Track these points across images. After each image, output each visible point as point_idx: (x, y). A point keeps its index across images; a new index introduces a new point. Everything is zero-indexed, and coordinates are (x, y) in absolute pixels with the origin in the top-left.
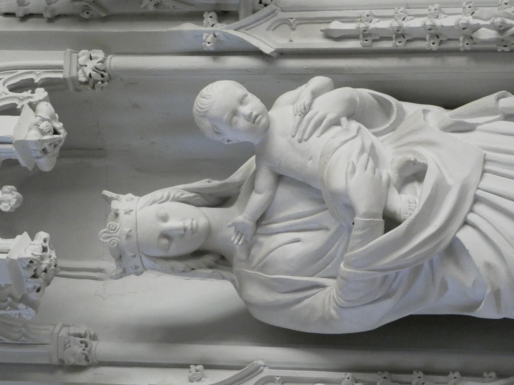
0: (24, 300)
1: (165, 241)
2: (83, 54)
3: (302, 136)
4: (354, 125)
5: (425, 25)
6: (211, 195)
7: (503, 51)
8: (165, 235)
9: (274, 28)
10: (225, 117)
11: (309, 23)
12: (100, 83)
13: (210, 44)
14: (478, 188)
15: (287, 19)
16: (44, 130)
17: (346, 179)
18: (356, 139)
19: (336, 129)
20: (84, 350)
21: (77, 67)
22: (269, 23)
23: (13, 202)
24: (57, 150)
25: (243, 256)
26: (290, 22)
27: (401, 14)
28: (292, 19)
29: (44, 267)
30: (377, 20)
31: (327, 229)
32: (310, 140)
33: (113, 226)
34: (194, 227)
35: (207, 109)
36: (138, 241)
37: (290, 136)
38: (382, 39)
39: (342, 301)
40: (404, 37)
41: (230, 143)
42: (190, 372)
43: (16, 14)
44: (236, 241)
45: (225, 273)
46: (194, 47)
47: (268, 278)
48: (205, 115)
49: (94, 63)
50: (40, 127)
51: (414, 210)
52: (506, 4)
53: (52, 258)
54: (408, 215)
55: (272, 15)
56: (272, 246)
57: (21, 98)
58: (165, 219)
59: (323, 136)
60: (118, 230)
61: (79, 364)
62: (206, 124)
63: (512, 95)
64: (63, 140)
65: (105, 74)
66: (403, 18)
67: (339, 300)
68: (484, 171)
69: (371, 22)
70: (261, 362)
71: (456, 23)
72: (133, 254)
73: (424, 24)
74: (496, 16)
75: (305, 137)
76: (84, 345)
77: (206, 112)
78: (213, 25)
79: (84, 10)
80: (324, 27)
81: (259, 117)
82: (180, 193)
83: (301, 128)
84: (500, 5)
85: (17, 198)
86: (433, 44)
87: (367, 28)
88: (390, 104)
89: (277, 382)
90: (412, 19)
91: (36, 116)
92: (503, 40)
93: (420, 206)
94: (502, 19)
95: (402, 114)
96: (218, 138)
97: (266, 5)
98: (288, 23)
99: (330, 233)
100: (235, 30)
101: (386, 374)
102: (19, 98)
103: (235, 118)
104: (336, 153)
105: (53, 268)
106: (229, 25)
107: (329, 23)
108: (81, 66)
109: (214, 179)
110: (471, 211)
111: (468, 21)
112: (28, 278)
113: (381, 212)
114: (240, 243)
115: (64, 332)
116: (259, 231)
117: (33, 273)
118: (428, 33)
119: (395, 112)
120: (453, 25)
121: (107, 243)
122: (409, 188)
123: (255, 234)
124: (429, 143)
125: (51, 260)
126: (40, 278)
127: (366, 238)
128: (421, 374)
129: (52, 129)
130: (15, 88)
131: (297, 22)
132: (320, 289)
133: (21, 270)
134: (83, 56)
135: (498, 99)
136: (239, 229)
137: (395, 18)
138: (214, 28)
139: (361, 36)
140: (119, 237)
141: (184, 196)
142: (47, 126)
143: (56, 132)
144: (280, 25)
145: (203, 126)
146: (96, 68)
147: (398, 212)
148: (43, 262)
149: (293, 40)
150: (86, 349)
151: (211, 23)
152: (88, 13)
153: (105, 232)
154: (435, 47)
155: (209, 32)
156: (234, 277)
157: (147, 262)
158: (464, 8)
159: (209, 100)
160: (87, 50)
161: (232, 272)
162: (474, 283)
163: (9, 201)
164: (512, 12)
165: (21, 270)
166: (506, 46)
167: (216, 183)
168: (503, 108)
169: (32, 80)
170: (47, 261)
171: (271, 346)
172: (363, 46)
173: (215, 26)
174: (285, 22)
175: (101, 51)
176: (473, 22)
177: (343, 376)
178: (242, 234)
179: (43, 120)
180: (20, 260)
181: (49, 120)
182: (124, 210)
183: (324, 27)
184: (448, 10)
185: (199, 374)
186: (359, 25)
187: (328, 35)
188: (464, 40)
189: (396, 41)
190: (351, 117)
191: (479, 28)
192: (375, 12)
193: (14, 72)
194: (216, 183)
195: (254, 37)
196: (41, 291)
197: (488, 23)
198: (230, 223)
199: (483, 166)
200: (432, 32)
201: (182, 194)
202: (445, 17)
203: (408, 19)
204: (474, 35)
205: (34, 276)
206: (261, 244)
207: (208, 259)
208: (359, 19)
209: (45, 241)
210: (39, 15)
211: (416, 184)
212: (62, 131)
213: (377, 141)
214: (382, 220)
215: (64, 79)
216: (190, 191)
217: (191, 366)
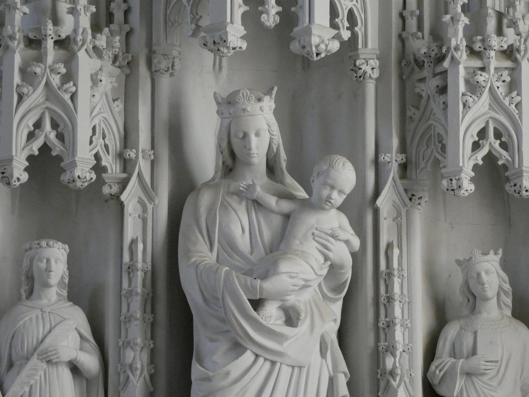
1: (241, 135)
2: (375, 63)
3: (317, 236)
5: (396, 319)
6: (275, 161)
7: (378, 373)
8: (246, 136)
9: (395, 206)
10: (330, 181)
11: (398, 232)
12: (355, 75)
13: (383, 160)
14: (281, 364)
15: (401, 215)
16: (319, 47)
17: (286, 273)
18: (315, 275)
19: (321, 259)
20: (163, 69)
21: (367, 58)
22: (397, 201)
23: (267, 24)
24: (306, 55)
25: (232, 189)
26: (399, 217)
27: (404, 299)
28: (401, 219)
29: (222, 49)
30: (400, 282)
31: (252, 253)
32: (314, 242)
33: (251, 99)
34: (252, 155)
35: (335, 167)
36: (241, 117)
37: (317, 227)
38: (387, 286)
39: (201, 268)
40: (388, 302)
41: (312, 182)
42: (149, 150)
43: (405, 11)
44: (242, 185)
45: (219, 173)
46: (382, 148)
47: (217, 208)
48: (331, 166)
49: (369, 71)
50: (321, 44)
51: (265, 320)
52: (411, 375)
53: (228, 53)
54: (261, 316)
55: (404, 205)
56: (239, 213)
57: (343, 21)
58: (257, 134)
59: (317, 251)
60: (248, 102)
61: (153, 65)
63: (347, 381)
64: (311, 60)
65: (361, 79)
66: (401, 301)
67: (202, 265)
68: (293, 367)
69: (399, 278)
70: (157, 202)
71: (397, 341)
72: (232, 112)
73: (397, 317)
74: (401, 370)
75: (316, 238)
76: (166, 69)
77: (333, 167)
78: (396, 161)
79: (407, 62)
80: (395, 243)
81: (330, 204)
82: (276, 143)
83: (322, 235)
84: (410, 371)
85: (271, 26)
86: (383, 324)
87: (394, 276)
88: (341, 293)
89: (143, 214)
90: (400, 307)
91: (329, 40)
92: (385, 373)
93: (268, 325)
94: (399, 374)
95: (334, 301)
96: (315, 174)
97: (410, 199)
98: (399, 216)
99: (249, 255)
100: (393, 177)
101: (151, 295)
102: (343, 19)
103: (329, 188)
104: (305, 263)
105: (220, 55)
106: (396, 173)
107: (398, 247)
108: (367, 62)
109: (286, 164)
110: (266, 359)
111: (398, 349)
112: (213, 38)
113: (263, 297)
114: (241, 188)
115: (175, 53)
116: (250, 202)
117: (217, 42)
118: (390, 320)
119: (335, 297)
120: (396, 339)
121: (240, 95)
122: (281, 314)
123: (248, 199)
125: (226, 53)
126: (213, 46)
128: (151, 320)
129: (320, 52)
130: (351, 13)
131: (399, 222)
132: (209, 249)
133: (220, 33)
134: (376, 63)
135: (345, 373)
136: (251, 187)
137: (401, 295)
138: (394, 161)
139: (388, 271)
140: (244, 103)
141: (274, 145)
142: (322, 49)
143: (318, 54)
144: (397, 210)
145: (323, 164)
146: (365, 73)
147: (265, 308)
148: (225, 48)
149: (386, 220)
150: (163, 71)
151: (398, 160)
152: (405, 65)
153: (247, 93)
154: (381, 325)
155: (391, 158)
156: (217, 180)
157: (226, 122)
158: (408, 345)
159: (342, 170)
160: (378, 65)
161: (220, 179)
162: (215, 362)
163: (268, 20)
164: (405, 380)
165: (220, 33)
166: (381, 375)
167: (284, 165)
168: (338, 377)
169: (357, 25)
170: (225, 51)
172: (381, 272)
173: (396, 162)
174: (399, 214)
175: (378, 75)
176: (398, 353)
177: (148, 264)
178: (247, 190)
179: (327, 46)
180: (226, 33)
181: (326, 50)
182: (263, 106)
183: (395, 243)
184: (406, 333)
185: (147, 157)
186: (396, 270)
187: (389, 246)
188: (385, 346)
189: (385, 296)
190: (332, 267)
191: (393, 357)
192: (405, 280)
193: (362, 11)
194: (284, 165)
195: (388, 192)
196: (204, 46)
197: (397, 364)
198: (255, 181)
199: (296, 366)
200: (391, 322)
201: (275, 144)
202: (401, 331)
203: (401, 304)
204: (389, 353)
205: (214, 42)
206: (240, 203)
207: (229, 161)
208: (400, 269)
209: (240, 48)
210: (404, 29)
211: (283, 319)
212: (319, 58)
214: (258, 298)
215: (357, 49)
216: (278, 149)
217: (153, 151)
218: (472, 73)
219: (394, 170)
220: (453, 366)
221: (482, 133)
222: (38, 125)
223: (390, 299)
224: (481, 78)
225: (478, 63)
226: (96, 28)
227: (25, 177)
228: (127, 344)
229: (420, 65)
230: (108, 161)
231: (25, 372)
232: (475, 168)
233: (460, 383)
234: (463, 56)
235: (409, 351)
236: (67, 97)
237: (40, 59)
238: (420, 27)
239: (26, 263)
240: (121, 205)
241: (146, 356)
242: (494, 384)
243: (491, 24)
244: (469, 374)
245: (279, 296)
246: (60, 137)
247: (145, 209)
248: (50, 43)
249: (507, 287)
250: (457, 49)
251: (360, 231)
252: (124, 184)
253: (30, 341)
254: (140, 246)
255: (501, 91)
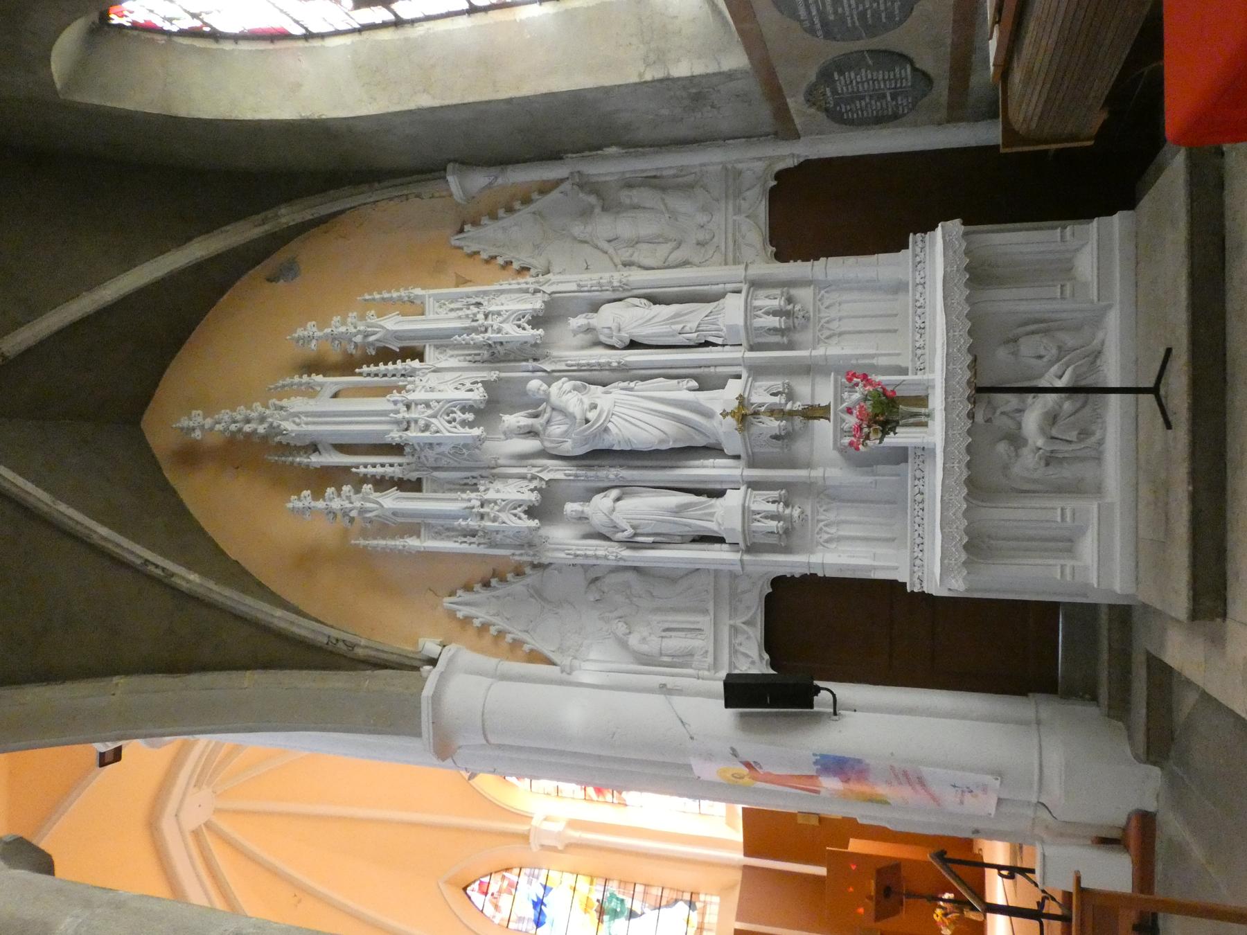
0: (477, 448)
4: (576, 392)
9: (551, 363)
19: (569, 394)
58: (519, 422)
62: (530, 393)
124: (598, 397)
127: (580, 426)
134: (493, 372)
171: (727, 840)
187: (567, 365)
213: (583, 397)
218: (493, 331)
219: (536, 364)
220: (616, 337)
221: (519, 326)
222: (515, 515)
223: (588, 364)
224: (495, 327)
225: (490, 329)
226: (477, 490)
227: (537, 521)
228: (607, 477)
229: (493, 354)
230: (532, 486)
231: (617, 521)
232: (533, 329)
233: (623, 334)
234: (487, 335)
235: (610, 357)
236: (503, 503)
237: (488, 514)
238: (479, 354)
239: (574, 521)
240: (550, 480)
241: (612, 469)
242: (623, 319)
243: (475, 324)
244: (619, 330)
245: (584, 412)
246: (520, 506)
247: (552, 470)
248: (482, 510)
249: (584, 315)
250: (484, 338)
251: (559, 378)
252: (541, 479)
253: (605, 519)
254: (567, 472)
255: (500, 319)
